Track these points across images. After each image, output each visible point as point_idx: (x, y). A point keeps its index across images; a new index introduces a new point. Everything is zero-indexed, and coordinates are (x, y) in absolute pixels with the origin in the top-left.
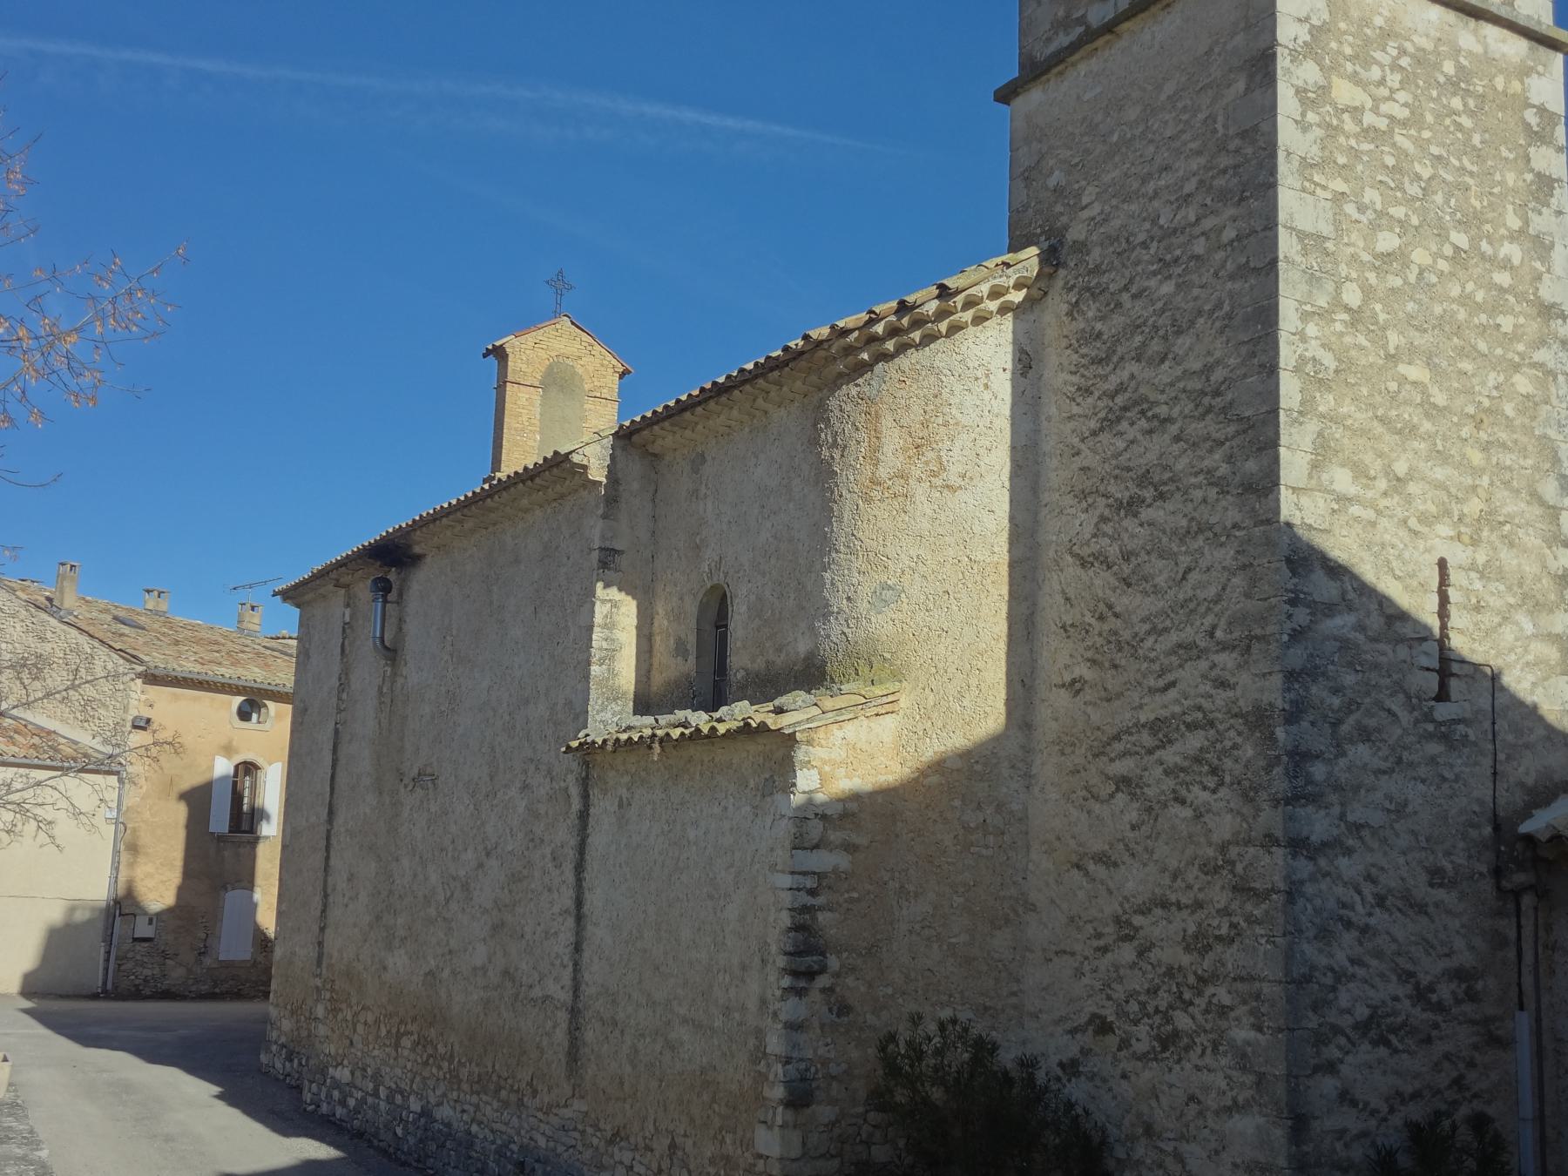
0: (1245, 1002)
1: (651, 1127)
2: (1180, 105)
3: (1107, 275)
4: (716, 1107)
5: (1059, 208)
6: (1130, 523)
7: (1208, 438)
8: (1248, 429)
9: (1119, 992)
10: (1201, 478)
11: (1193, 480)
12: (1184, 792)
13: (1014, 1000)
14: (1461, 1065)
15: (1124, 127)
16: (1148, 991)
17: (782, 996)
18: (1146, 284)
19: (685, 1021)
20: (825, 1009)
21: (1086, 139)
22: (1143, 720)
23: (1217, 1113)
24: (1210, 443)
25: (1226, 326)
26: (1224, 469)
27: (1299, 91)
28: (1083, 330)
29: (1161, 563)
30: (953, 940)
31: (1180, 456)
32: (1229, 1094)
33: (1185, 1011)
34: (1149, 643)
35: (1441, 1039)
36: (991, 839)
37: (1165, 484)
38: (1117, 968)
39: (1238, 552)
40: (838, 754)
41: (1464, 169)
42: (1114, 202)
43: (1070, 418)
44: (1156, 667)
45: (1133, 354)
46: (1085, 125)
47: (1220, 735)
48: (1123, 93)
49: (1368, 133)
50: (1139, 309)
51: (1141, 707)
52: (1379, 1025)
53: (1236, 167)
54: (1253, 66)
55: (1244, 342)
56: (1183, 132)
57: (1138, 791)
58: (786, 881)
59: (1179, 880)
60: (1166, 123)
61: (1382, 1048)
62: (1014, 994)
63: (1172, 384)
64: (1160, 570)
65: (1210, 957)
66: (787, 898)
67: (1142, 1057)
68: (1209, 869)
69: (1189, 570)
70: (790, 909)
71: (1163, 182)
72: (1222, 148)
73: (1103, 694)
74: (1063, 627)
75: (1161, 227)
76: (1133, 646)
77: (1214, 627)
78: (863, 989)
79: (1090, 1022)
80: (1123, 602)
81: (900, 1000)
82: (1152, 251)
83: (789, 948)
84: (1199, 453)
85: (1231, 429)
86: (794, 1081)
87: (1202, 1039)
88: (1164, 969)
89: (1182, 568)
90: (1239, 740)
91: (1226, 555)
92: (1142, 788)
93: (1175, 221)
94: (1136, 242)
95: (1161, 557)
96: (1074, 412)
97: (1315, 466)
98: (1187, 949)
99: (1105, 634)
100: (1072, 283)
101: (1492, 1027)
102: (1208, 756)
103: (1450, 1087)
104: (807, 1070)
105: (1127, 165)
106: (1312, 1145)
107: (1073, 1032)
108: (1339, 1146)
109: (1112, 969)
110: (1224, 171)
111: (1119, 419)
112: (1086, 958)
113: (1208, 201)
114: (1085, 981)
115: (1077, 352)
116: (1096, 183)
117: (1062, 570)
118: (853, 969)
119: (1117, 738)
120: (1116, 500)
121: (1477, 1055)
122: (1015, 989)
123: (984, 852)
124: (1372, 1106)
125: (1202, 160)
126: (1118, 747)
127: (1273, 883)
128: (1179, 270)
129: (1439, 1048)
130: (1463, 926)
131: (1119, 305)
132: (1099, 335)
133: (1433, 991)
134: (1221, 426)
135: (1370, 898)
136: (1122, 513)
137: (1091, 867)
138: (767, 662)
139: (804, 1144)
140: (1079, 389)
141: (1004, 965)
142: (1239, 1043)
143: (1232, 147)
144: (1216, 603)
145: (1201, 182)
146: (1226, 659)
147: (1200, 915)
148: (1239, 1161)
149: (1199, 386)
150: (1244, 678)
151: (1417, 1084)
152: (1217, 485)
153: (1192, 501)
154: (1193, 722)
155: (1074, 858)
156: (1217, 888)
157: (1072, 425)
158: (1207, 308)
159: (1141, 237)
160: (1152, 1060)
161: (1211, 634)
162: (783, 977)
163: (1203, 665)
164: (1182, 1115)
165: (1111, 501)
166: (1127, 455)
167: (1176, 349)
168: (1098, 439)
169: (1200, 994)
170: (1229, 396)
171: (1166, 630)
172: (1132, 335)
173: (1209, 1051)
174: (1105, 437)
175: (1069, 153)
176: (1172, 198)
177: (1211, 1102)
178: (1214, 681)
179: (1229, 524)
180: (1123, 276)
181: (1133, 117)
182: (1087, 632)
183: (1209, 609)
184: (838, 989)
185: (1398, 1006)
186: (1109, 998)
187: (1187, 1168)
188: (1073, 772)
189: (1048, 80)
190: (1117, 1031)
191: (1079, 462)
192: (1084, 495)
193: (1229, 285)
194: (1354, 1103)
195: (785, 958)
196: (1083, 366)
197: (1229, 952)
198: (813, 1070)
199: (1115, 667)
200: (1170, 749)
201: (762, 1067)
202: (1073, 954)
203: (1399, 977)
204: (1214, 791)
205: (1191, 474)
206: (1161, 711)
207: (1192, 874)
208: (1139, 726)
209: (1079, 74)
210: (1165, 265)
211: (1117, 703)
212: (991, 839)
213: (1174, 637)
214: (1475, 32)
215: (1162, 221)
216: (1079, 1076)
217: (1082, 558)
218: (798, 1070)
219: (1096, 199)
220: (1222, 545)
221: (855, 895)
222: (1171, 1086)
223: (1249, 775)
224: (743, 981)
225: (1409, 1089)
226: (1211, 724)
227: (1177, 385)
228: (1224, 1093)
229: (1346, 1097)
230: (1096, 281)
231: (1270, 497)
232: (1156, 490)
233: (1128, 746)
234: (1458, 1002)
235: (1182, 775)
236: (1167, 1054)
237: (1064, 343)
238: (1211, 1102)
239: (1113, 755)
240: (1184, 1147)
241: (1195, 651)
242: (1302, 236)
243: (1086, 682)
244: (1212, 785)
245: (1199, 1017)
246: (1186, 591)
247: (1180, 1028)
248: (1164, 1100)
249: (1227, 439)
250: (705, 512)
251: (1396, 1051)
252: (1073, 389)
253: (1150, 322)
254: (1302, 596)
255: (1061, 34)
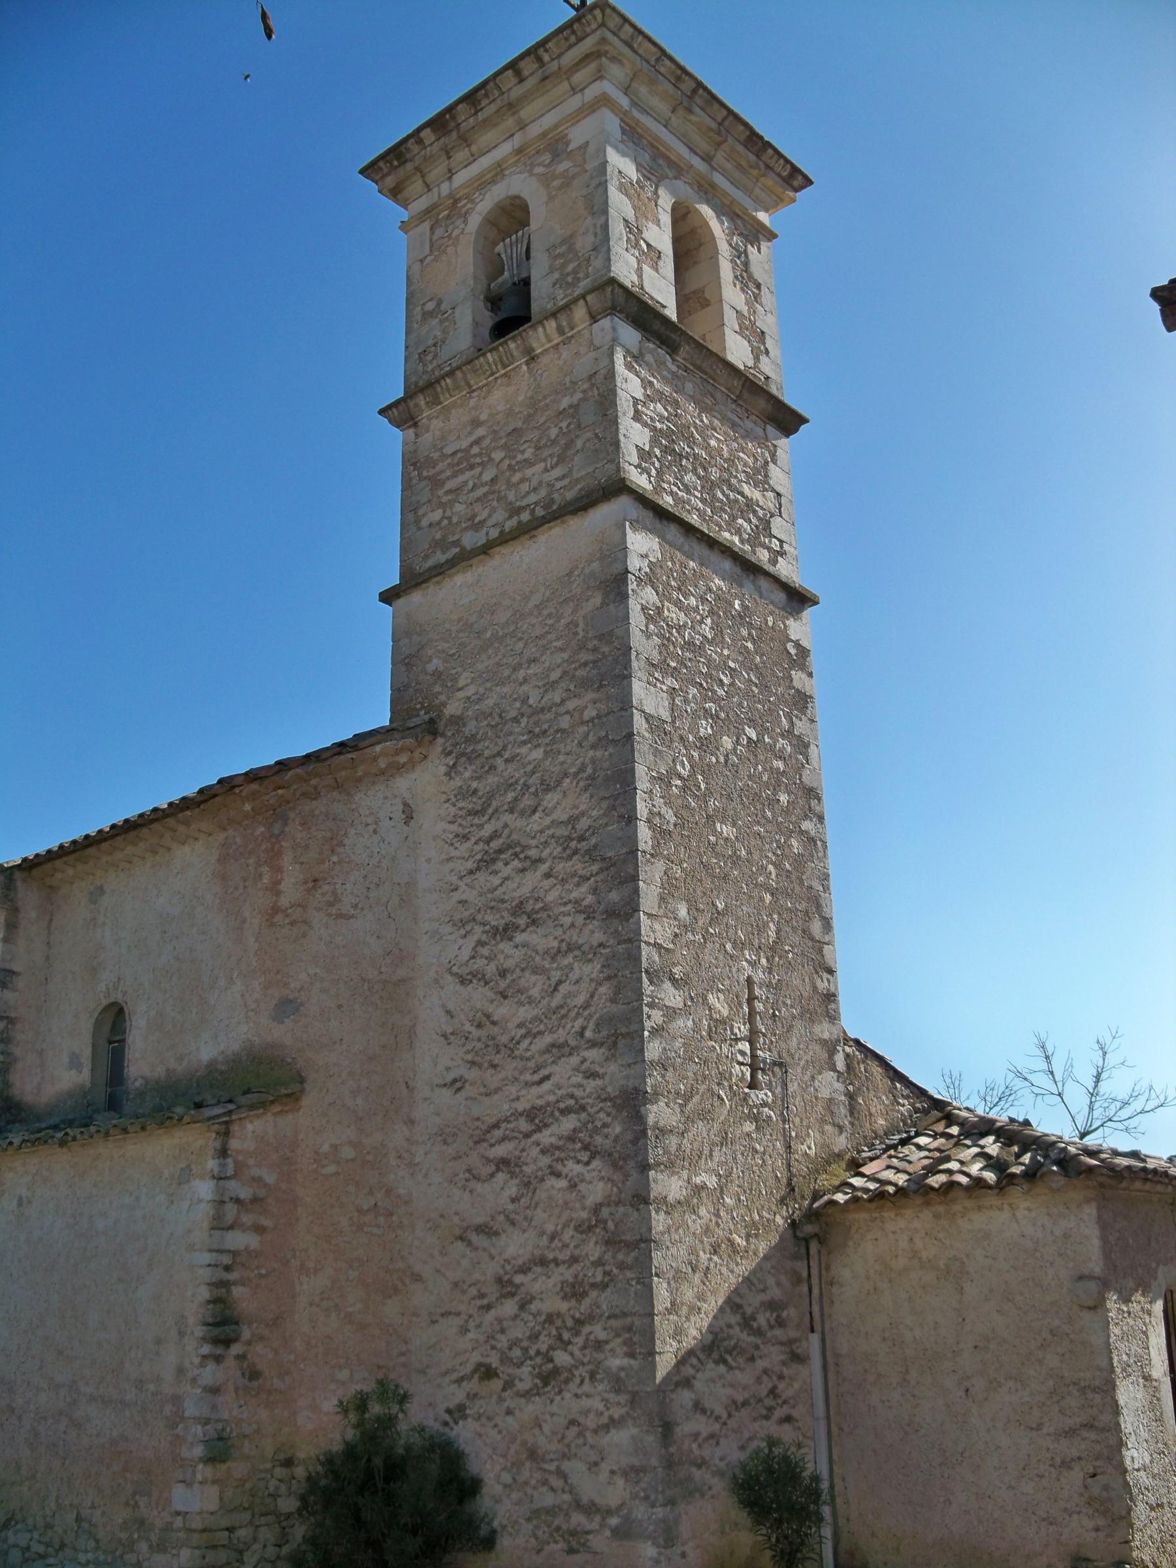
0: (618, 1335)
1: (53, 1506)
2: (545, 612)
3: (482, 743)
4: (128, 1475)
5: (437, 689)
6: (506, 946)
7: (574, 875)
8: (610, 867)
9: (503, 1341)
10: (569, 907)
11: (562, 909)
12: (559, 1167)
13: (403, 1359)
14: (775, 1378)
15: (496, 627)
16: (530, 1338)
17: (201, 1363)
18: (518, 751)
19: (92, 1399)
20: (239, 1373)
21: (461, 635)
22: (520, 1109)
23: (595, 1431)
24: (576, 879)
25: (589, 785)
26: (590, 899)
27: (644, 608)
28: (461, 787)
29: (534, 978)
30: (350, 1309)
31: (550, 890)
32: (606, 1414)
33: (566, 1351)
34: (525, 1044)
35: (761, 1357)
36: (382, 1220)
37: (537, 912)
38: (499, 1320)
39: (603, 966)
40: (250, 1145)
41: (751, 681)
42: (488, 685)
43: (450, 859)
44: (531, 1064)
45: (506, 807)
46: (461, 624)
47: (592, 1117)
48: (494, 600)
49: (689, 645)
50: (512, 771)
51: (518, 1098)
52: (719, 1348)
53: (595, 662)
54: (607, 586)
55: (605, 798)
56: (548, 633)
57: (517, 1170)
58: (207, 1258)
59: (556, 1241)
60: (533, 625)
61: (721, 1366)
62: (403, 1354)
63: (542, 832)
64: (535, 985)
65: (586, 1302)
66: (205, 1274)
67: (526, 1394)
68: (585, 1229)
69: (559, 982)
70: (209, 1284)
71: (532, 671)
72: (582, 647)
73: (482, 1090)
74: (445, 1036)
75: (530, 706)
76: (510, 1048)
77: (584, 1029)
78: (270, 1356)
79: (475, 1371)
80: (501, 1011)
81: (302, 1366)
82: (523, 725)
83: (210, 1320)
84: (567, 886)
85: (595, 868)
86: (213, 1440)
87: (582, 1371)
88: (543, 1317)
89: (554, 981)
90: (608, 1120)
91: (593, 969)
92: (521, 1167)
93: (543, 702)
94: (508, 717)
95: (534, 972)
96: (453, 854)
97: (662, 899)
98: (565, 1297)
99: (483, 1040)
100: (449, 749)
101: (794, 1347)
102: (580, 1135)
103: (768, 1396)
104: (223, 1429)
105: (500, 657)
106: (675, 1447)
107: (459, 1381)
108: (694, 1446)
109: (495, 1323)
110: (585, 664)
111: (494, 861)
112: (470, 1316)
113: (572, 687)
114: (470, 1335)
115: (455, 806)
116: (471, 670)
117: (442, 988)
118: (261, 1338)
119: (496, 1126)
120: (492, 927)
121: (785, 1369)
122: (404, 1349)
123: (376, 1231)
124: (717, 1413)
125: (565, 656)
126: (498, 1133)
127: (641, 1235)
128: (547, 741)
129: (761, 1364)
130: (773, 1267)
131: (493, 768)
132: (475, 791)
133: (755, 1319)
134: (587, 864)
135: (708, 1247)
136: (498, 937)
137: (474, 1237)
138: (168, 1070)
139: (221, 1499)
140: (457, 836)
141: (395, 1329)
142: (614, 1370)
143: (590, 645)
144: (585, 1008)
145: (565, 673)
146: (593, 1054)
147: (577, 1267)
148: (615, 1468)
149: (566, 833)
150: (612, 1068)
151: (746, 1395)
152: (584, 913)
153: (562, 925)
154: (566, 1107)
155: (457, 1232)
156: (591, 1244)
157: (451, 865)
158: (573, 770)
159: (513, 713)
160: (535, 1395)
161: (581, 1034)
162: (202, 1346)
163: (575, 1060)
164: (563, 1438)
165: (487, 928)
166: (501, 890)
167: (545, 803)
168: (474, 877)
169: (578, 1334)
170: (593, 841)
171: (541, 1033)
172: (506, 791)
173: (587, 1381)
174: (481, 877)
175: (447, 645)
176: (540, 684)
177: (591, 1422)
178: (584, 1073)
179: (595, 944)
180: (496, 744)
181: (503, 620)
182: (467, 1038)
183: (578, 1014)
184: (249, 1356)
185: (731, 1332)
186: (493, 1348)
187: (569, 1482)
188: (455, 1159)
189: (428, 588)
190: (501, 1375)
191: (457, 896)
192: (463, 923)
193: (591, 753)
194: (704, 1411)
195: (204, 1328)
196: (461, 817)
197: (603, 1295)
198: (228, 1429)
199: (494, 1066)
200: (547, 1132)
201: (180, 1429)
202: (458, 1314)
203: (732, 1308)
204: (587, 1163)
205: (560, 904)
206: (537, 1101)
207: (569, 1233)
208: (517, 1115)
209: (455, 584)
210: (533, 737)
211: (496, 1097)
212: (382, 1220)
213: (548, 1039)
214: (753, 582)
215: (531, 701)
216: (466, 1418)
217: (461, 976)
218: (216, 1430)
219: (472, 682)
220: (590, 961)
221: (263, 1272)
222: (552, 1415)
223: (618, 1148)
224: (158, 1354)
225: (740, 1399)
226: (583, 1108)
227: (547, 832)
228: (602, 1413)
229: (698, 1407)
230: (471, 748)
231: (631, 920)
232: (529, 918)
233: (507, 1132)
234: (771, 1327)
235: (557, 1153)
236: (549, 1388)
237: (444, 797)
238: (591, 1422)
239: (493, 1141)
240: (566, 1466)
241: (567, 1050)
242: (648, 718)
243: (466, 1081)
244: (585, 1159)
245: (577, 1353)
246: (557, 999)
247: (559, 1365)
248: (546, 1428)
249: (592, 875)
250: (103, 937)
251: (731, 1368)
252: (451, 836)
253: (522, 782)
254: (657, 1001)
255: (439, 553)
